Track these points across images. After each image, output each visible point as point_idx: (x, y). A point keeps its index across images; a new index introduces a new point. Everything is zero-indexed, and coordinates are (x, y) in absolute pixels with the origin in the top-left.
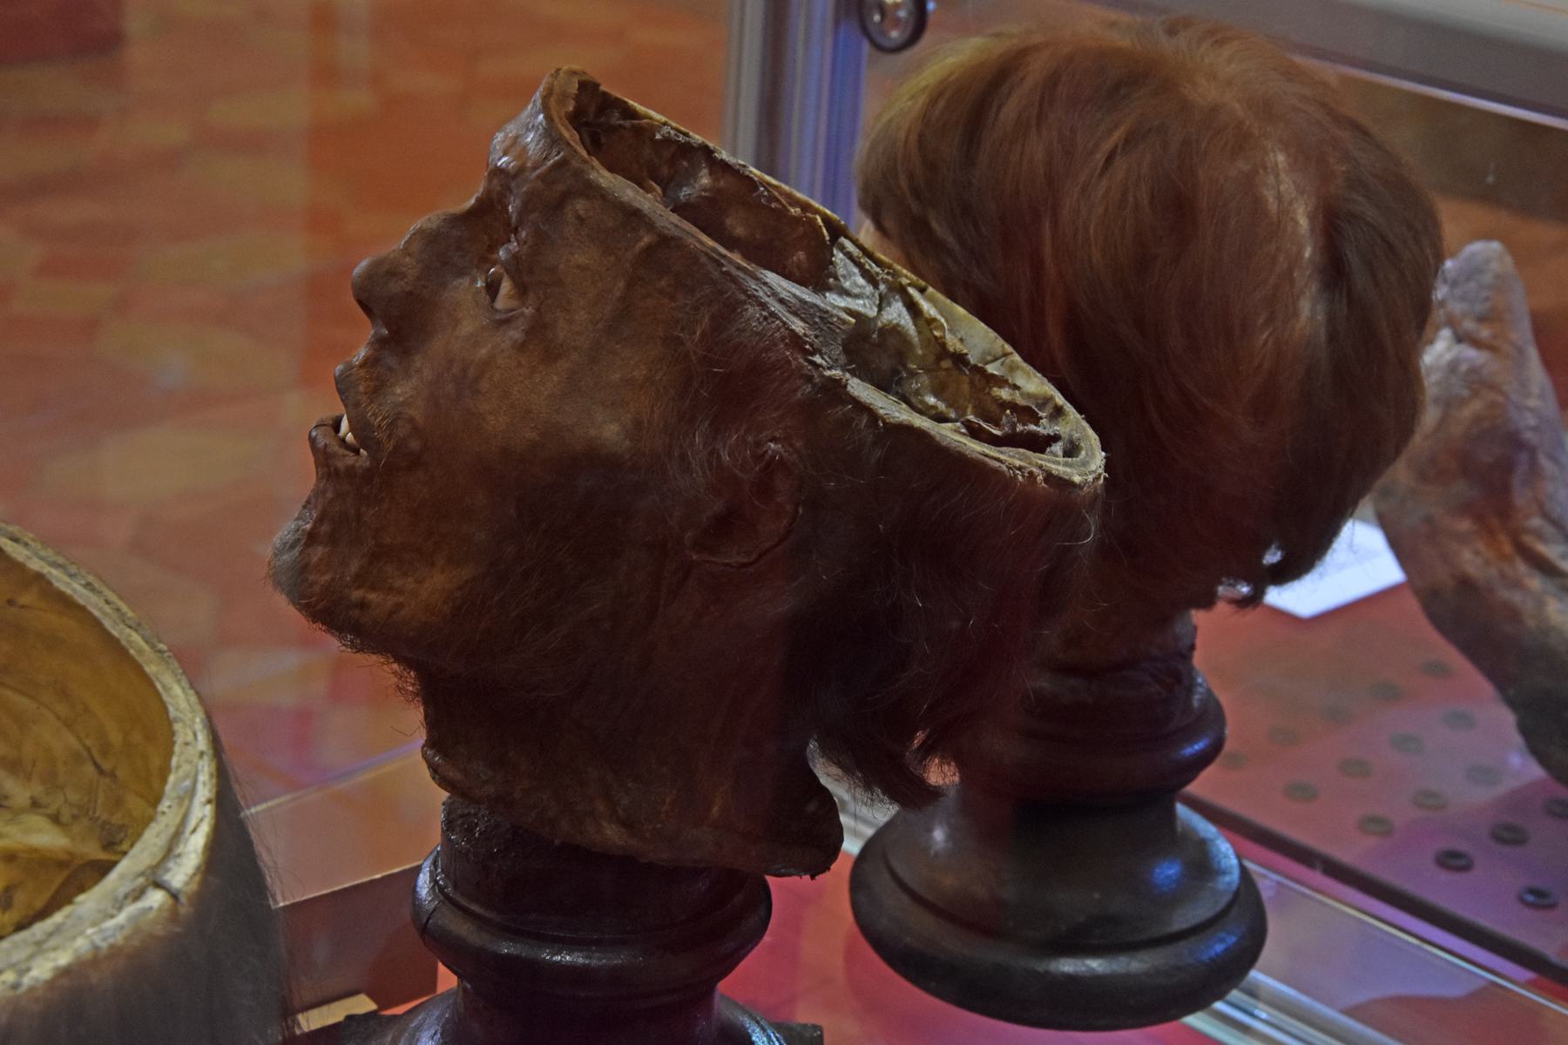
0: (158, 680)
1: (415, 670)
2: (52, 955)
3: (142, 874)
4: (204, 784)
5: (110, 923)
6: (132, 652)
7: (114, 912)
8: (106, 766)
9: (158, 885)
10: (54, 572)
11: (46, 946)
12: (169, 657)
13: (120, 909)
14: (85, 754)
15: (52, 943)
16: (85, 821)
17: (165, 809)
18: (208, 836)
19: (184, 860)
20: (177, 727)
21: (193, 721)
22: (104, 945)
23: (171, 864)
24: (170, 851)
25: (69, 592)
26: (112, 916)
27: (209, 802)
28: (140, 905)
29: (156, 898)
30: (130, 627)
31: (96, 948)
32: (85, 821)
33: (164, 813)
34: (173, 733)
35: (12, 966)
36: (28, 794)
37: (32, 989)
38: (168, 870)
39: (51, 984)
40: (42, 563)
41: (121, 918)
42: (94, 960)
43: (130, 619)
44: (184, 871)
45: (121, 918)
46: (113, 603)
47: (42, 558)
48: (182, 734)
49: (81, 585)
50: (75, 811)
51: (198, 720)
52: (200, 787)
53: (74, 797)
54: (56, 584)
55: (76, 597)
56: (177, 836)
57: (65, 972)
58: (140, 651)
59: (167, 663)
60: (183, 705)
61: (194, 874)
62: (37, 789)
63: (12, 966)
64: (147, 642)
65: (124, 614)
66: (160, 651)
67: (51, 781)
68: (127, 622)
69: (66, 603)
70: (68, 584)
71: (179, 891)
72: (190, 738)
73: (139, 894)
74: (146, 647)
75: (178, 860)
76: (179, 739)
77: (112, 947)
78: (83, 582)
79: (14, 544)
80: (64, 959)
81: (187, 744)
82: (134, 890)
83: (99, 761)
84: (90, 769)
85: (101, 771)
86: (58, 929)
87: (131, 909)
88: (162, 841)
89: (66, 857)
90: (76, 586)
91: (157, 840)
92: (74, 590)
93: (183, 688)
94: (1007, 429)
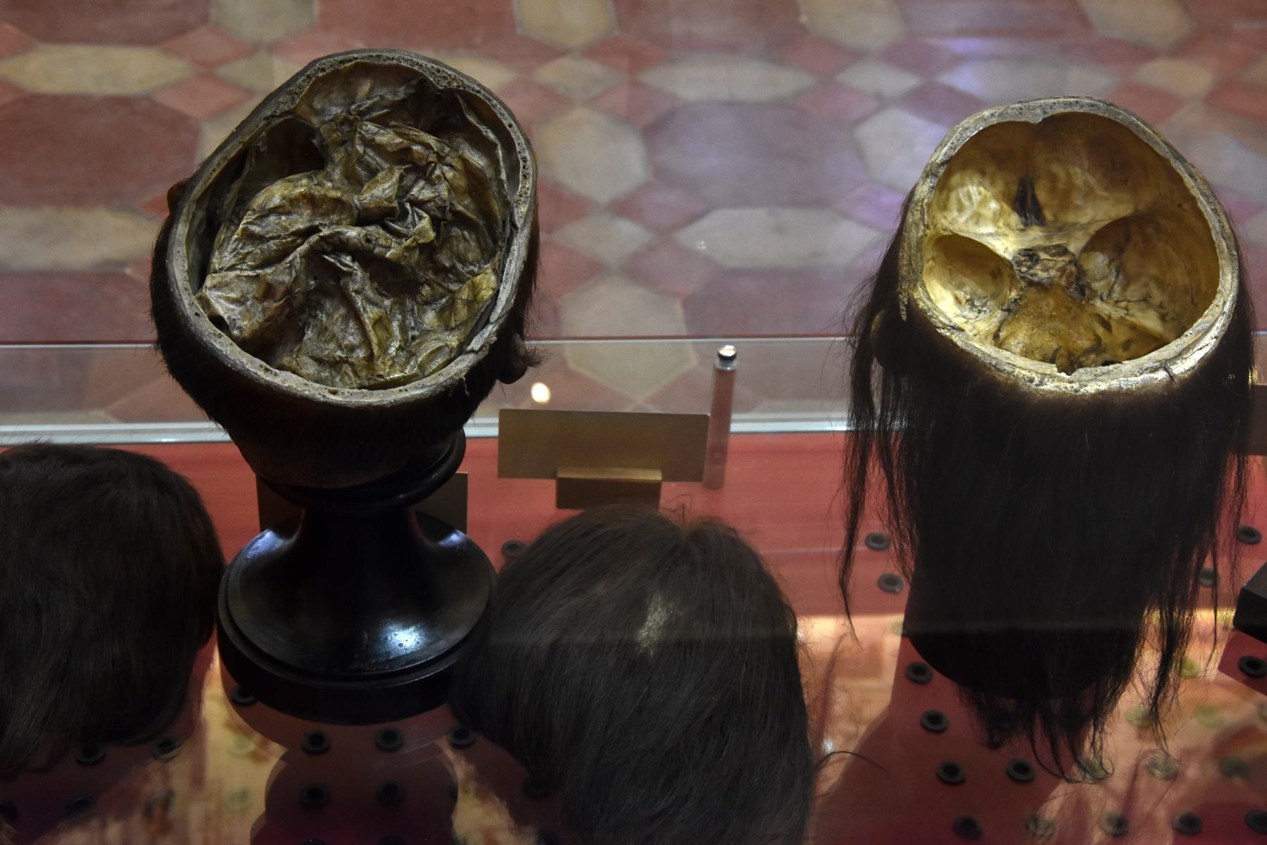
0: (1222, 268)
1: (498, 339)
2: (1100, 383)
3: (1160, 361)
4: (1218, 328)
5: (1134, 379)
6: (1218, 251)
7: (1138, 374)
8: (1196, 300)
9: (1166, 369)
10: (1201, 198)
11: (1099, 378)
12: (1235, 259)
13: (1141, 374)
14: (1190, 290)
15: (1102, 377)
16: (1176, 323)
17: (1189, 335)
18: (1206, 354)
19: (1188, 361)
20: (1218, 296)
21: (1229, 295)
22: (1125, 387)
23: (1179, 362)
24: (1179, 355)
25: (1203, 210)
26: (1136, 376)
27: (1216, 337)
28: (1152, 375)
29: (1161, 375)
30: (1224, 238)
31: (1121, 388)
32: (1176, 323)
33: (1187, 336)
34: (1214, 297)
35: (1079, 381)
36: (1161, 299)
37: (1083, 395)
38: (1175, 364)
39: (1093, 396)
40: (1198, 192)
41: (1139, 379)
42: (1118, 393)
43: (1226, 233)
44: (1181, 368)
45: (1139, 379)
46: (1222, 222)
47: (1199, 189)
48: (1218, 300)
49: (1211, 209)
50: (1175, 316)
51: (1231, 295)
52: (1214, 328)
53: (1178, 309)
54: (1199, 204)
55: (1205, 214)
56: (1188, 349)
57: (1102, 393)
58: (1222, 252)
59: (1233, 261)
60: (1228, 286)
61: (1189, 370)
62: (1165, 298)
63: (1079, 381)
64: (1228, 248)
65: (1224, 230)
66: (1232, 255)
67: (1172, 298)
68: (1225, 235)
69: (1200, 215)
70: (1205, 206)
71: (1175, 375)
72: (1221, 304)
73: (1155, 370)
74: (1226, 250)
75: (1184, 361)
76: (1215, 302)
77: (1129, 389)
78: (1213, 208)
79: (1190, 178)
80: (1103, 386)
81: (1217, 306)
82: (1152, 368)
83: (1194, 296)
84: (1189, 298)
85: (1193, 301)
86: (1108, 373)
87: (1146, 376)
88: (1178, 349)
89: (1158, 336)
90: (1209, 209)
91: (1176, 348)
92: (1206, 211)
93: (1233, 277)
94: (914, 426)
